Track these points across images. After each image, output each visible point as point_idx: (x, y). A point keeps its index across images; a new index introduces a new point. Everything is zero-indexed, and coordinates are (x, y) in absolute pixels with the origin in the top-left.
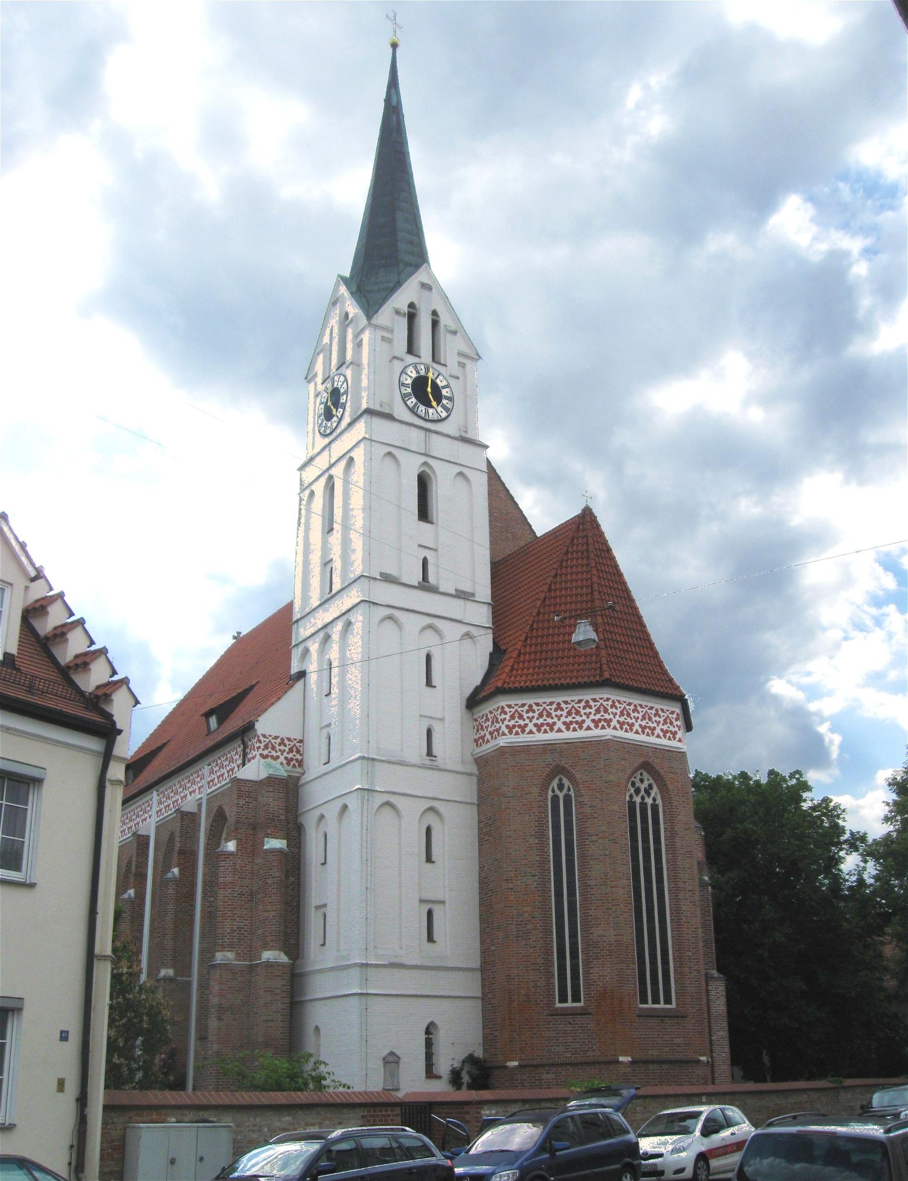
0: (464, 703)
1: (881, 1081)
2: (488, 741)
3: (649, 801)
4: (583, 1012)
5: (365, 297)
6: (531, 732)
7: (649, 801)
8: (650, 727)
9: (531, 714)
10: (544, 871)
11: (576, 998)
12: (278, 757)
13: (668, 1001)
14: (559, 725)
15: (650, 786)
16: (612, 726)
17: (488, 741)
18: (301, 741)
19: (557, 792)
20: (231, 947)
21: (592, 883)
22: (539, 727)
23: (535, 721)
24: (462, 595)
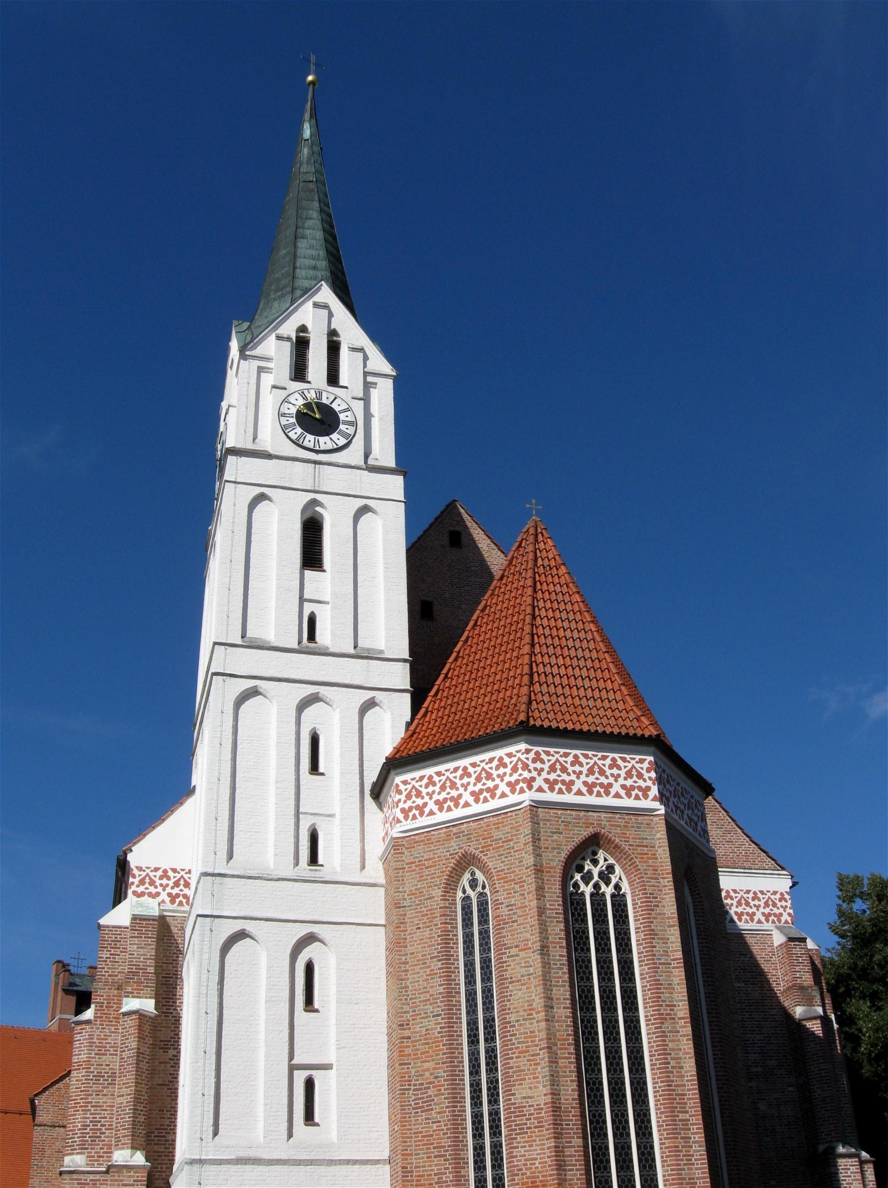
3: (608, 891)
7: (608, 891)
12: (158, 894)
16: (535, 788)
18: (190, 872)
20: (83, 1147)
22: (440, 804)
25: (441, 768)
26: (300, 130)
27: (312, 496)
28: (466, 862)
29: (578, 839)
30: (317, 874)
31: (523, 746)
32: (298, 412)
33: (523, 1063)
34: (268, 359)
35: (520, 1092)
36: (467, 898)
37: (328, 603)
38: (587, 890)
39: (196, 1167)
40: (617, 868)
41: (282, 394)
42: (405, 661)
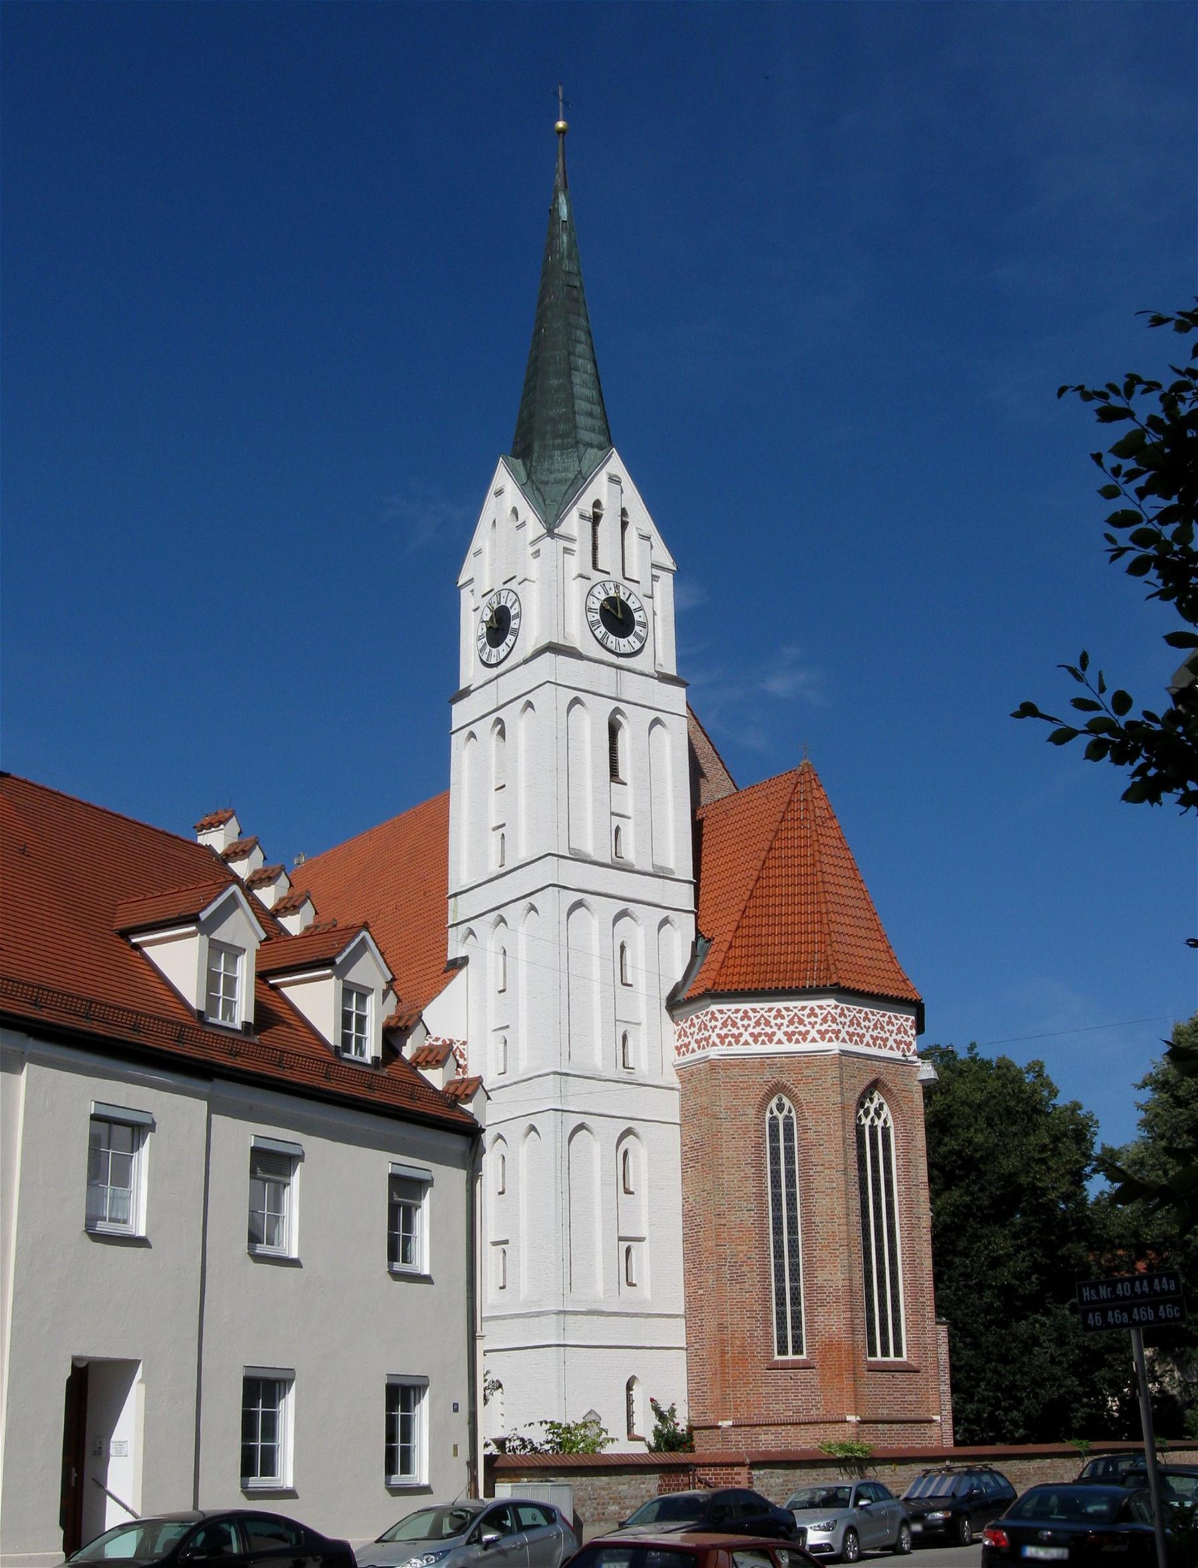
0: (664, 1004)
1: (1170, 1443)
2: (694, 1051)
4: (807, 1366)
5: (538, 489)
6: (746, 1043)
7: (879, 1123)
8: (858, 1035)
9: (746, 1022)
10: (762, 1205)
11: (798, 1350)
13: (898, 1352)
14: (780, 1035)
15: (881, 1105)
17: (694, 1051)
18: (464, 1043)
19: (776, 1113)
21: (817, 1220)
22: (755, 1037)
23: (750, 1030)
24: (660, 874)
25: (757, 1006)
26: (554, 211)
27: (616, 704)
28: (778, 1089)
29: (866, 1083)
30: (632, 1077)
31: (833, 1002)
32: (602, 607)
33: (825, 1254)
34: (572, 540)
35: (821, 1277)
36: (774, 1118)
37: (629, 818)
38: (866, 1122)
39: (561, 1316)
40: (886, 1107)
41: (588, 584)
42: (690, 882)
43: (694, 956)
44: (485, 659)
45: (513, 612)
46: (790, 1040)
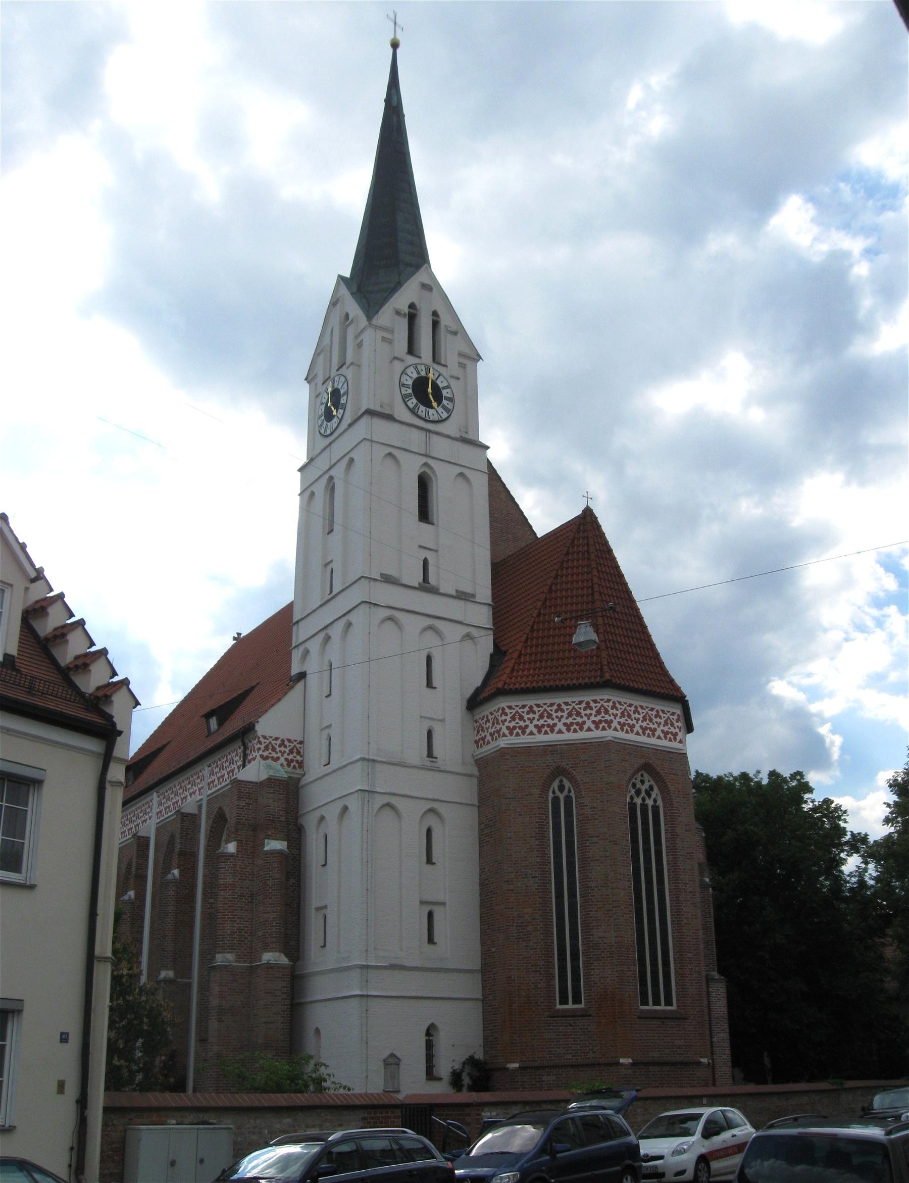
3: (650, 802)
4: (584, 1014)
7: (650, 802)
9: (531, 716)
11: (577, 1000)
12: (278, 759)
15: (651, 788)
17: (488, 742)
18: (301, 743)
19: (558, 793)
21: (593, 884)
22: (539, 728)
23: (535, 722)
24: (462, 596)
30: (435, 765)
43: (492, 665)
44: (322, 432)
45: (342, 392)
46: (568, 730)
